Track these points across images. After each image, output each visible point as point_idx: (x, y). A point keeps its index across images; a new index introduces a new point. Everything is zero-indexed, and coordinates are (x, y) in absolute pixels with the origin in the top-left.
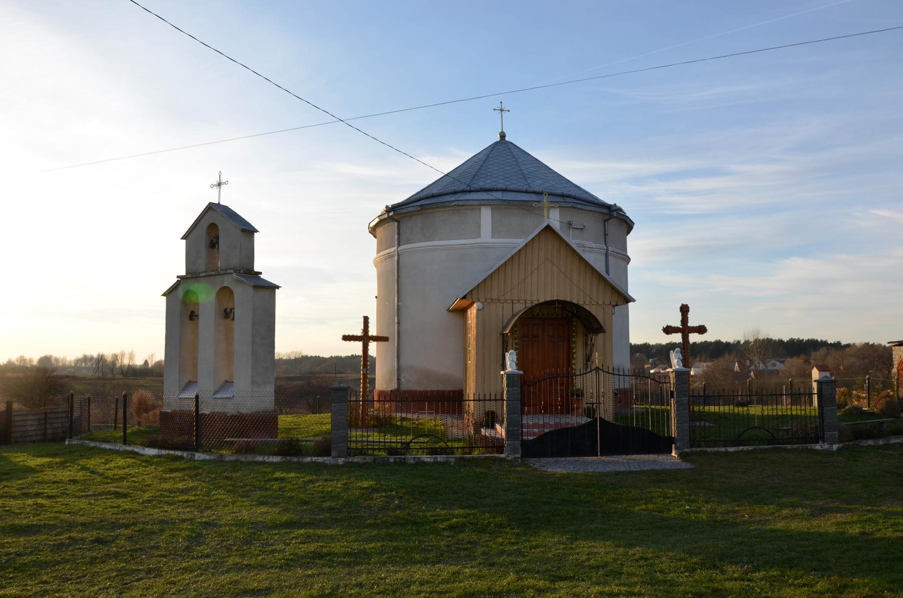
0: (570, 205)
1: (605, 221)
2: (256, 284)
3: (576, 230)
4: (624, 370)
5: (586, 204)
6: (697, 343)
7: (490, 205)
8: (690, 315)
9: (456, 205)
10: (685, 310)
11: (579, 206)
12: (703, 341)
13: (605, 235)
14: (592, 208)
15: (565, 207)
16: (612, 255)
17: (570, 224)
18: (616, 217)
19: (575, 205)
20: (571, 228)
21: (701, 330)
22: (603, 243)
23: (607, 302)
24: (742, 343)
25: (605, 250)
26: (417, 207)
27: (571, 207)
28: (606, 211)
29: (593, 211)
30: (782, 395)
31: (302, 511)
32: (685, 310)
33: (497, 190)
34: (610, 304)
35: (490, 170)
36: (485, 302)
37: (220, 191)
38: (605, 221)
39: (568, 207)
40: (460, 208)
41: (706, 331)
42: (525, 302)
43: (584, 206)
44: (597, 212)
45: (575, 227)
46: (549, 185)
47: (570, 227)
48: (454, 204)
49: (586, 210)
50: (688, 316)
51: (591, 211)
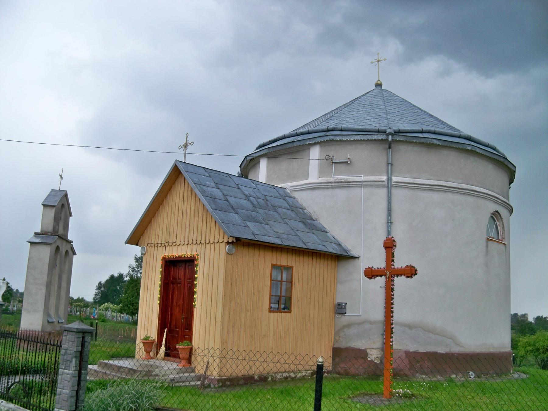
11: (345, 138)
15: (324, 142)
44: (368, 140)
45: (338, 161)
49: (350, 141)
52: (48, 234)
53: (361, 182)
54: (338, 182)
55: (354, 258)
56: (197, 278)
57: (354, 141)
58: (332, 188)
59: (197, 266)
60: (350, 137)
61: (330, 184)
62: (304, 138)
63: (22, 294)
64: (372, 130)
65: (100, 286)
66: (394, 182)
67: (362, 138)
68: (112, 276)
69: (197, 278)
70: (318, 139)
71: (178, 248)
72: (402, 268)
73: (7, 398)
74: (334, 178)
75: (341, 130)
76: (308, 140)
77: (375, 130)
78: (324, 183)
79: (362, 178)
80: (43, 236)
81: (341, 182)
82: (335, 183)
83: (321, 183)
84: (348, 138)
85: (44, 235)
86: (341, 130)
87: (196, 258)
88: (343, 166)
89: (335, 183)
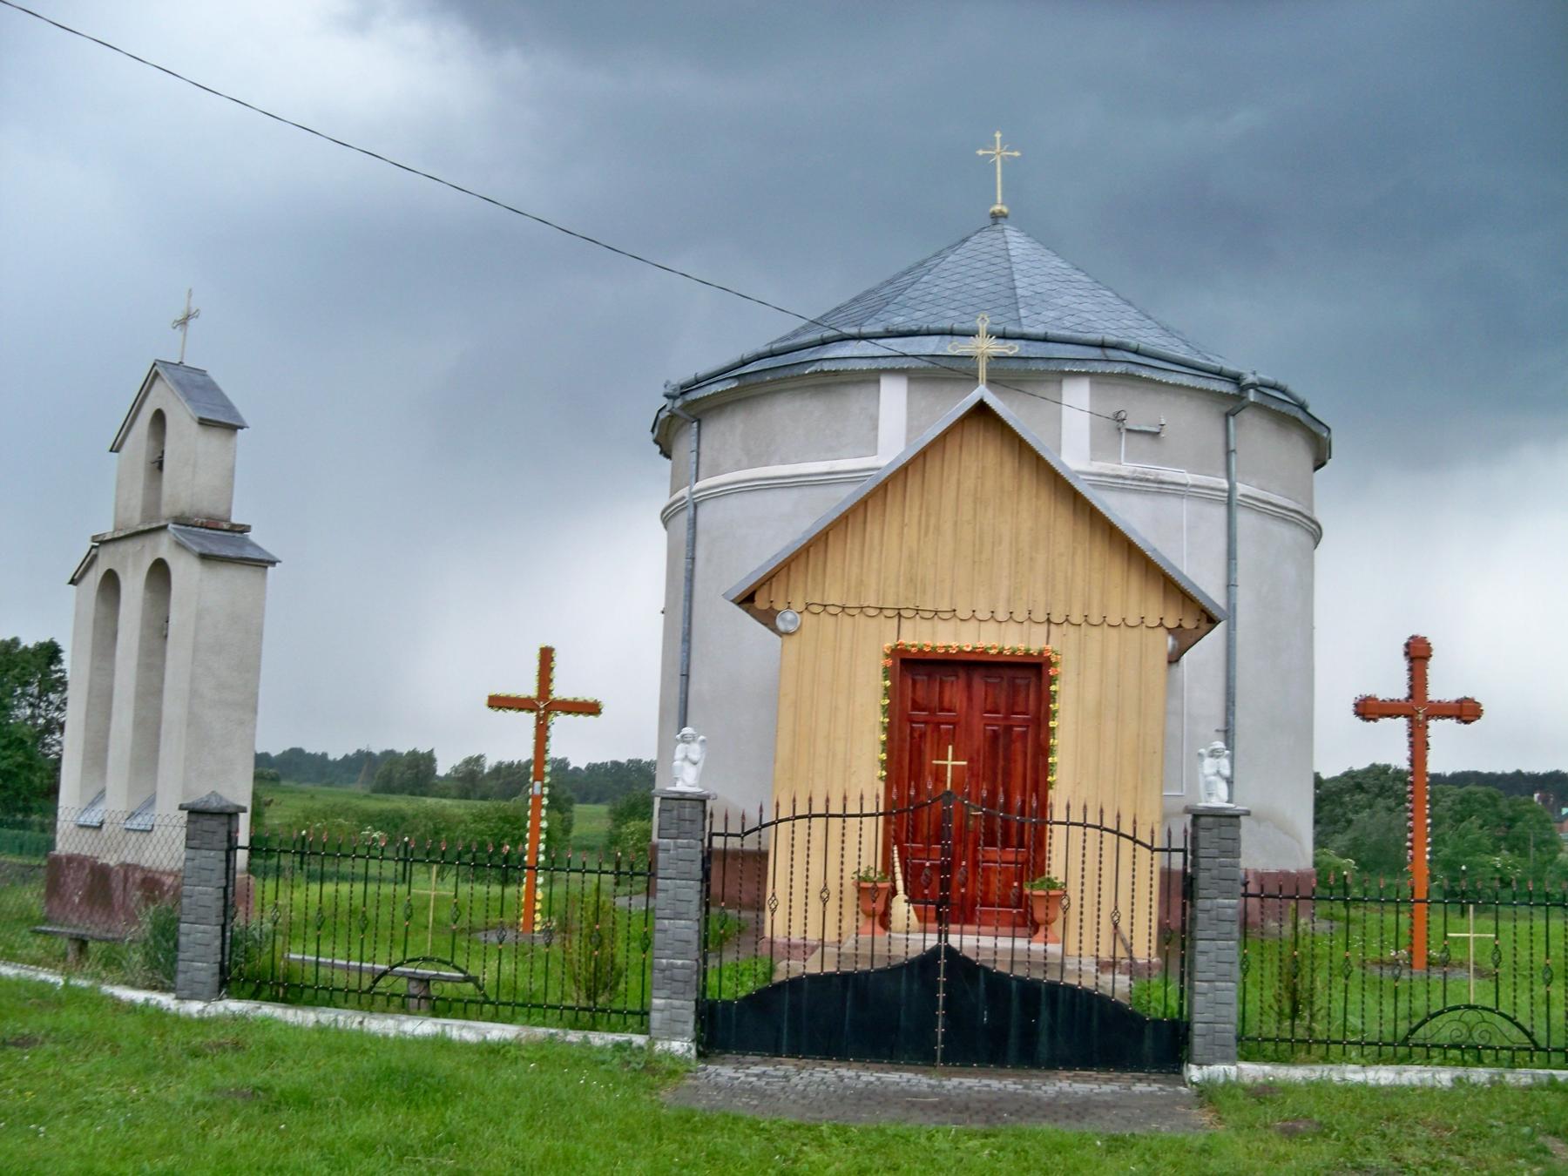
0: (1118, 368)
1: (1227, 415)
2: (206, 551)
3: (1135, 438)
4: (743, 817)
5: (1210, 375)
6: (331, 757)
7: (1086, 374)
8: (1434, 669)
9: (816, 372)
10: (1417, 653)
11: (1145, 373)
12: (351, 752)
13: (1228, 452)
14: (1186, 380)
15: (1103, 374)
16: (1250, 508)
17: (1118, 419)
18: (1255, 405)
19: (1132, 369)
20: (1123, 431)
21: (1466, 711)
22: (1222, 473)
23: (1153, 620)
24: (570, 768)
25: (1223, 491)
26: (731, 381)
27: (1120, 375)
28: (1227, 388)
29: (1188, 387)
30: (303, 959)
31: (213, 1091)
32: (1417, 653)
33: (929, 333)
34: (1161, 625)
35: (935, 290)
36: (805, 613)
37: (185, 335)
38: (1227, 415)
39: (1111, 375)
40: (829, 379)
41: (1479, 717)
42: (900, 615)
43: (1162, 373)
44: (1201, 390)
45: (1137, 428)
46: (1078, 321)
47: (1119, 429)
48: (812, 369)
49: (1167, 384)
50: (1428, 671)
51: (1180, 386)
52: (219, 527)
53: (1185, 485)
54: (1141, 480)
55: (264, 563)
56: (1056, 711)
57: (1175, 386)
58: (1123, 490)
59: (1052, 680)
60: (1168, 374)
61: (1120, 481)
62: (1027, 345)
63: (651, 764)
64: (1207, 368)
65: (1374, 765)
66: (1243, 495)
67: (1186, 380)
68: (61, 651)
69: (1056, 711)
70: (1096, 364)
71: (902, 625)
72: (1000, 653)
73: (1013, 1040)
74: (1126, 468)
75: (1136, 352)
76: (1070, 363)
77: (1214, 369)
78: (1106, 476)
79: (1188, 478)
80: (202, 530)
81: (1147, 480)
82: (1133, 479)
83: (1100, 475)
84: (1157, 376)
85: (206, 528)
86: (1136, 352)
87: (1053, 660)
88: (1144, 442)
89: (1133, 479)
